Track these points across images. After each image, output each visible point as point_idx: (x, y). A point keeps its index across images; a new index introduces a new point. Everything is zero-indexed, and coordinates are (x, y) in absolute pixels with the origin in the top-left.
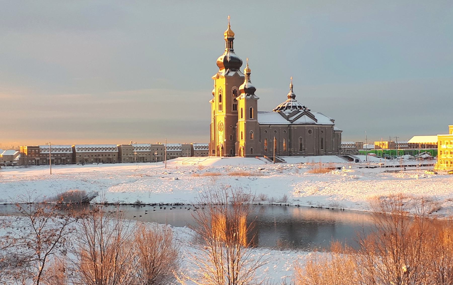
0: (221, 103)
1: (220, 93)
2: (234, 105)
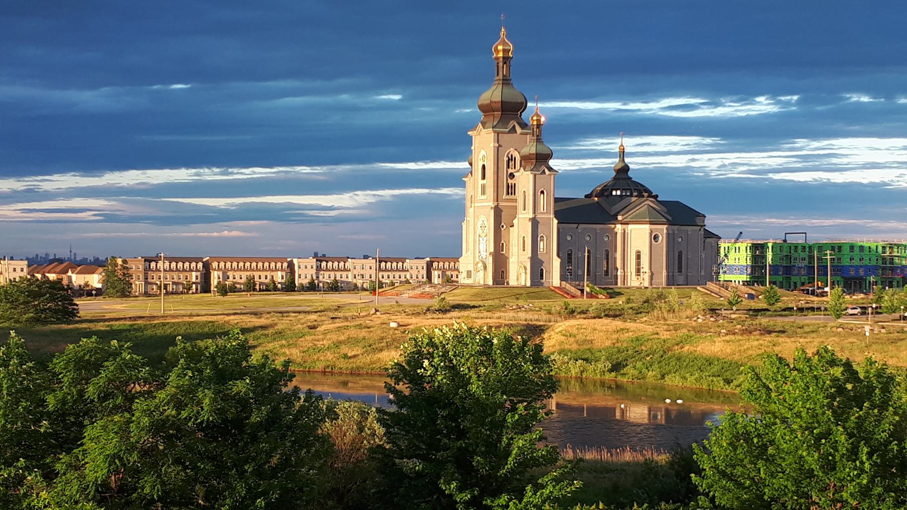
0: (484, 182)
1: (484, 161)
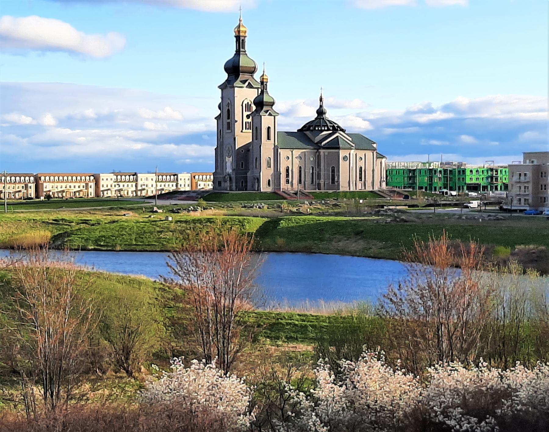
0: (229, 121)
2: (246, 122)
